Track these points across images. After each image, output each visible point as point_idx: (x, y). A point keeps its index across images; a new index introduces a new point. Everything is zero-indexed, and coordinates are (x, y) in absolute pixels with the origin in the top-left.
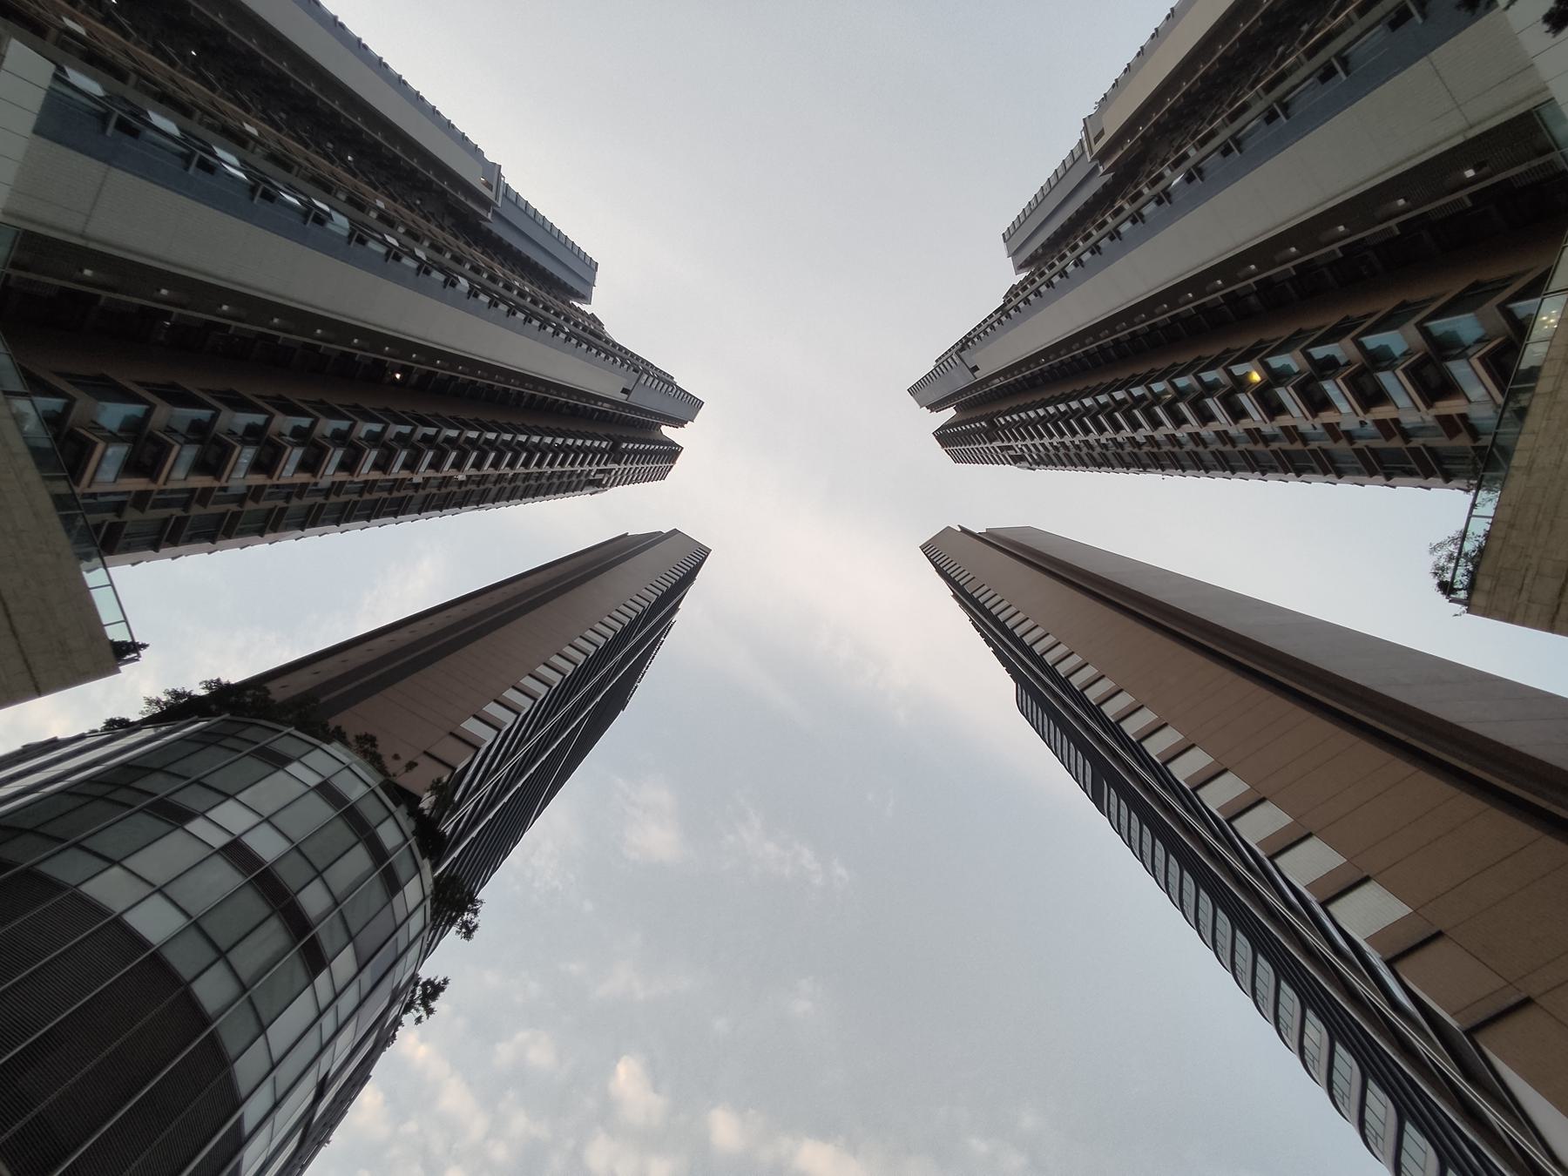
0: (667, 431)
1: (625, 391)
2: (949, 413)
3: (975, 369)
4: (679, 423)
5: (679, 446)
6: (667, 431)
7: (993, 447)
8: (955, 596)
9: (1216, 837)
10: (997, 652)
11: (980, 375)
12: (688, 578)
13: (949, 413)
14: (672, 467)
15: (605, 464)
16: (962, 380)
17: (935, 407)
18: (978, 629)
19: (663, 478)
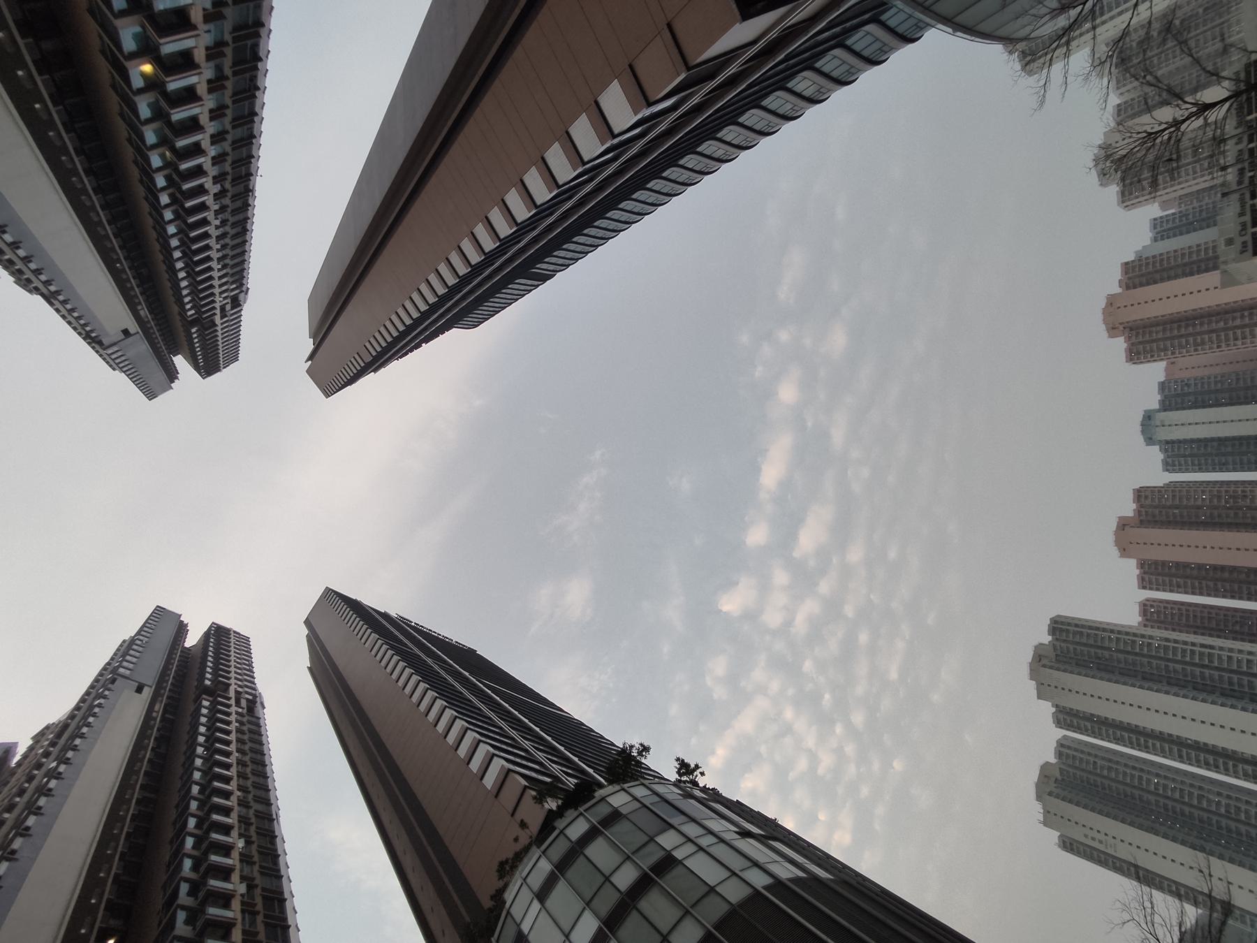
0: (192, 640)
1: (139, 690)
2: (180, 361)
3: (126, 333)
4: (182, 629)
5: (211, 626)
6: (192, 640)
7: (222, 324)
8: (375, 371)
9: (570, 198)
10: (427, 340)
11: (133, 327)
12: (356, 607)
13: (180, 361)
14: (235, 632)
15: (229, 699)
16: (140, 347)
17: (172, 374)
18: (406, 354)
19: (247, 639)
